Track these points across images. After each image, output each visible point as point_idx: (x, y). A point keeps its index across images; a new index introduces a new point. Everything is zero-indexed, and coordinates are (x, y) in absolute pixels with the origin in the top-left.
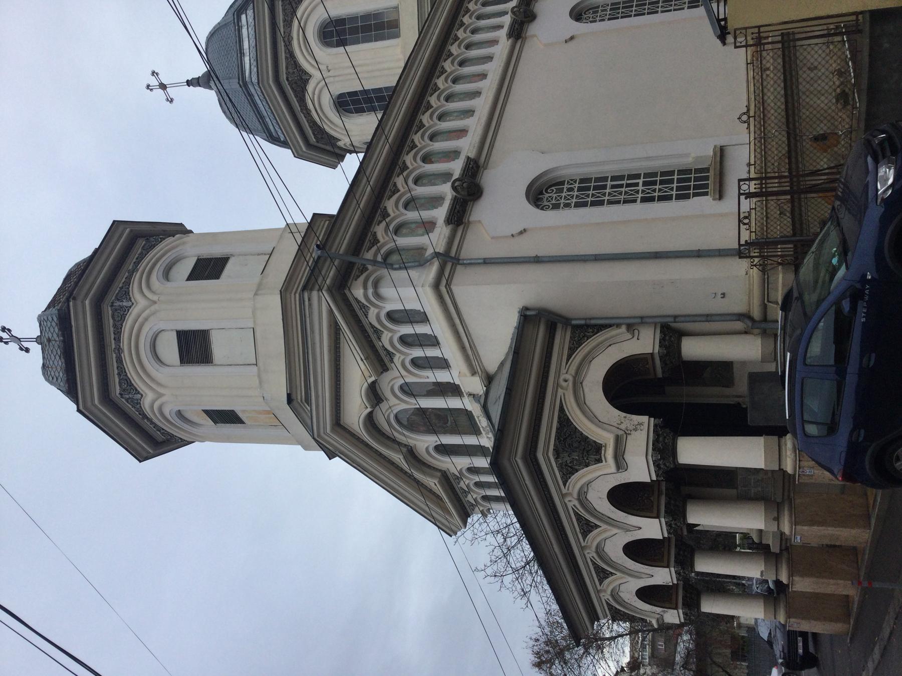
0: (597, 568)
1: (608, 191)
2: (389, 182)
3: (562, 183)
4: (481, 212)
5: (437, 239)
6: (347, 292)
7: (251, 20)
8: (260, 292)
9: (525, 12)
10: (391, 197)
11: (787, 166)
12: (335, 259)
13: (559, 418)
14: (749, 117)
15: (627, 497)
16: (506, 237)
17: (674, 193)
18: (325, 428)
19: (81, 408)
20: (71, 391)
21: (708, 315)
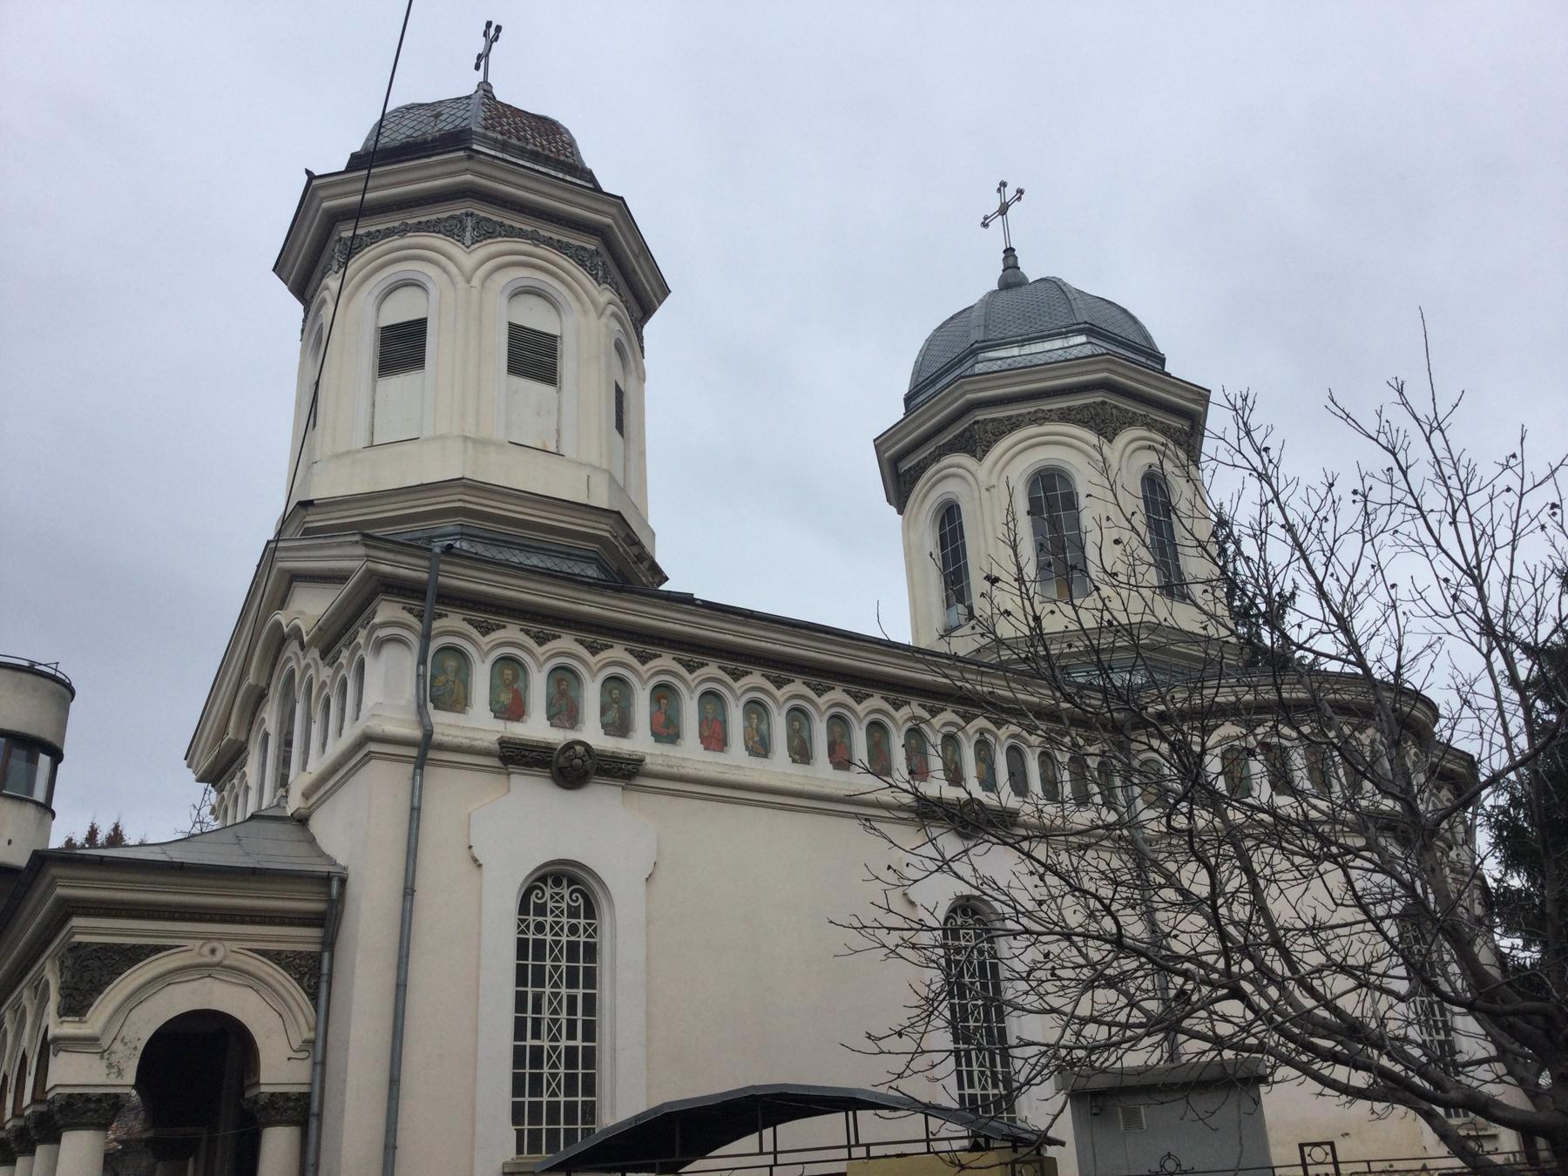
4: (532, 794)
7: (1075, 352)
8: (470, 444)
13: (141, 947)
20: (357, 162)
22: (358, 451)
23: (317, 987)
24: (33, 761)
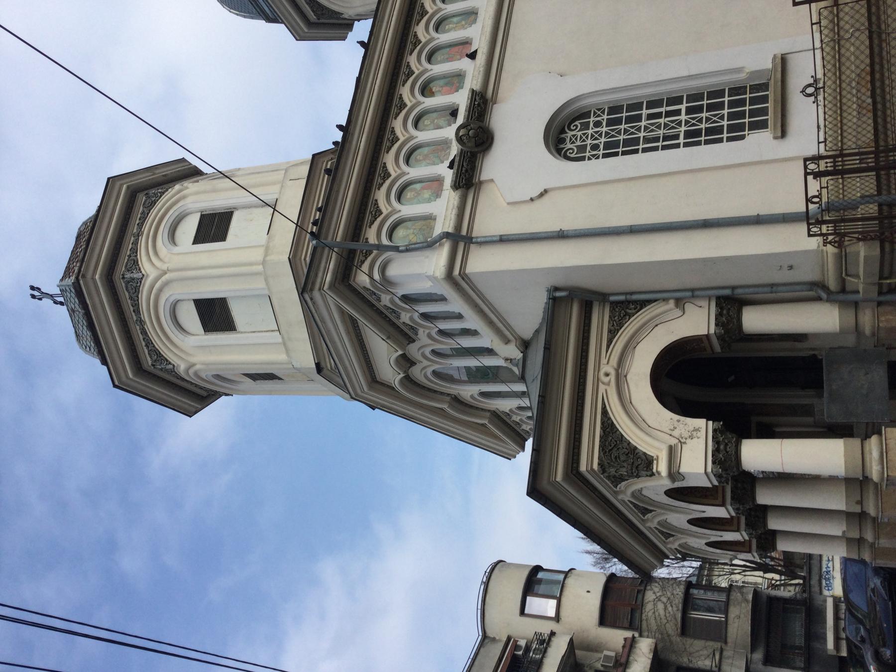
1: (643, 123)
3: (587, 115)
4: (494, 167)
5: (444, 223)
6: (351, 282)
10: (389, 149)
11: (869, 85)
12: (346, 189)
13: (603, 423)
14: (816, 89)
17: (725, 123)
19: (117, 383)
22: (283, 338)
23: (635, 302)
24: (540, 581)
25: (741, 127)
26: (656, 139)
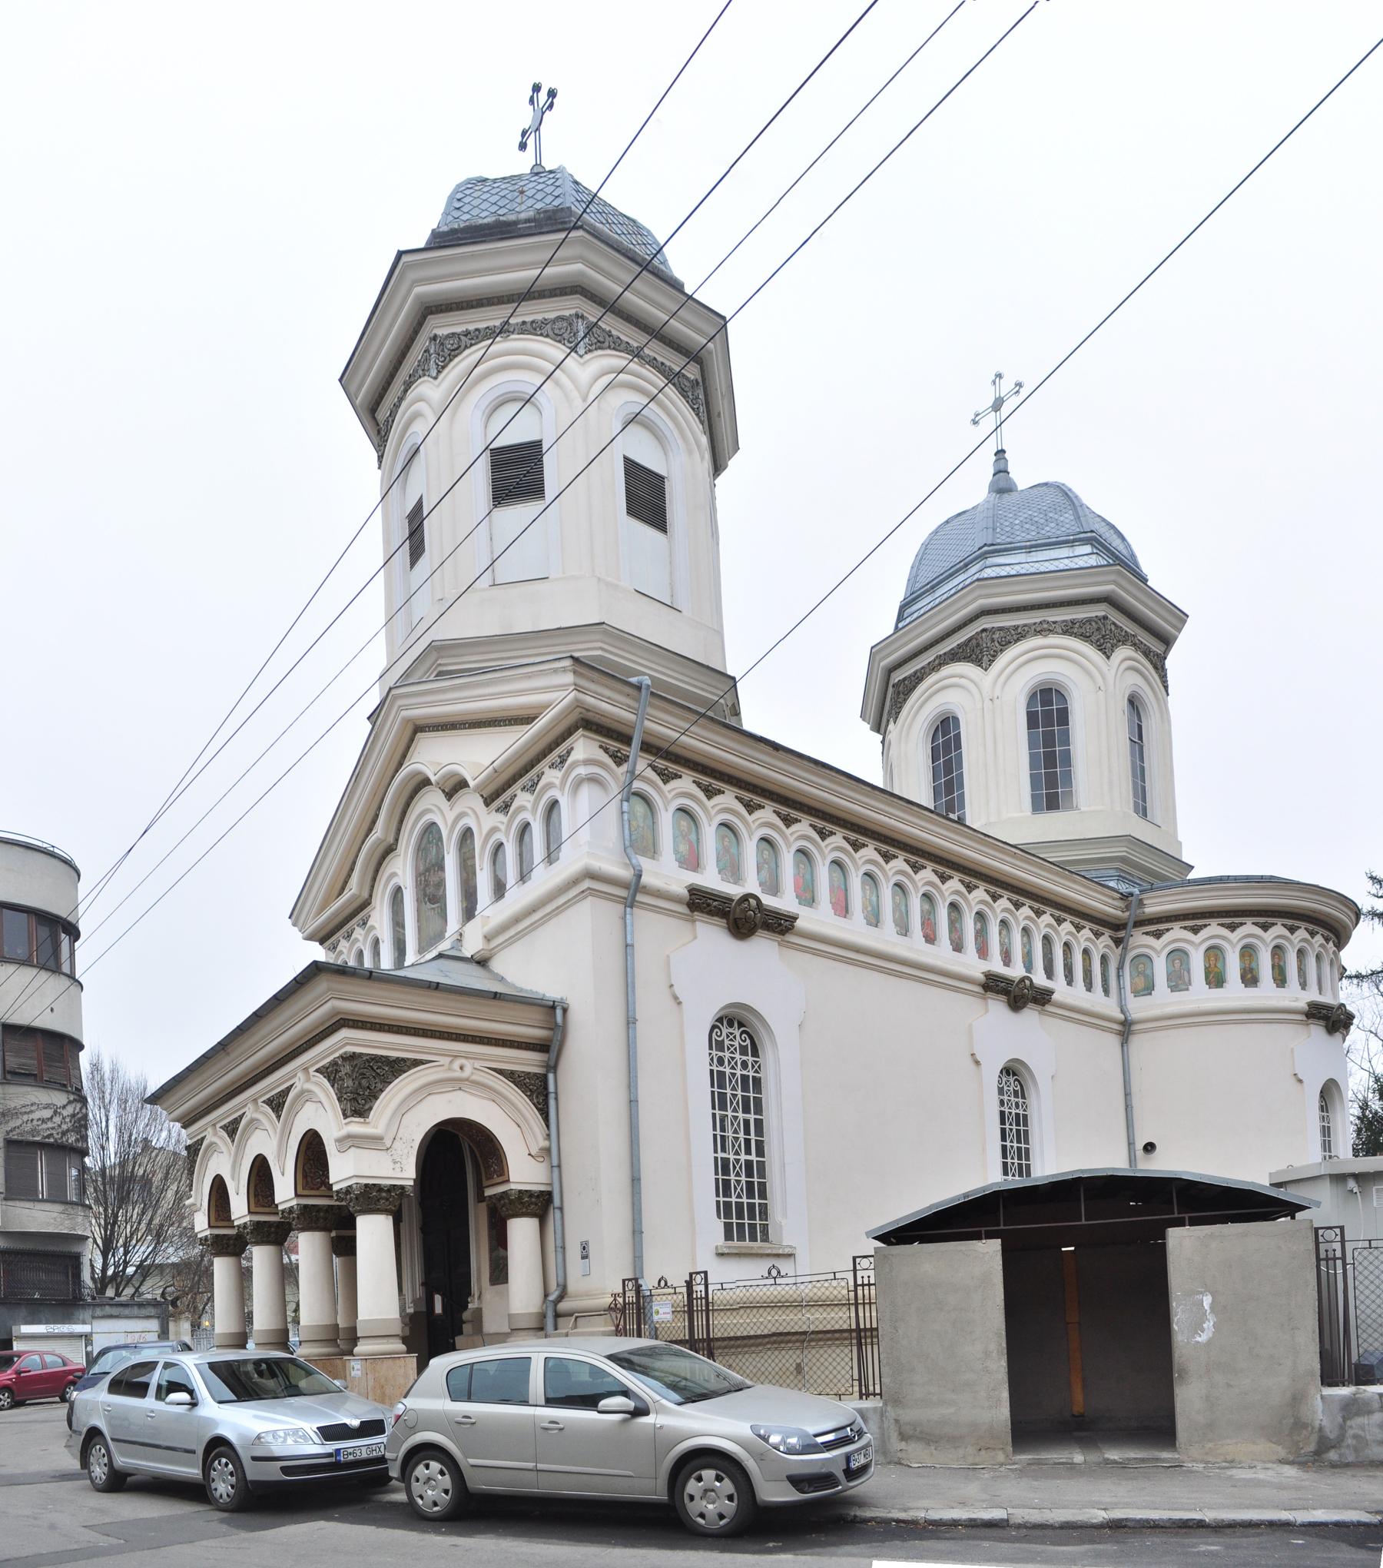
0: (236, 1122)
2: (765, 797)
4: (711, 935)
9: (1023, 996)
13: (403, 1060)
15: (312, 1155)
16: (669, 977)
17: (734, 1199)
18: (407, 708)
20: (441, 240)
21: (564, 1248)
25: (728, 1215)
26: (723, 1129)
